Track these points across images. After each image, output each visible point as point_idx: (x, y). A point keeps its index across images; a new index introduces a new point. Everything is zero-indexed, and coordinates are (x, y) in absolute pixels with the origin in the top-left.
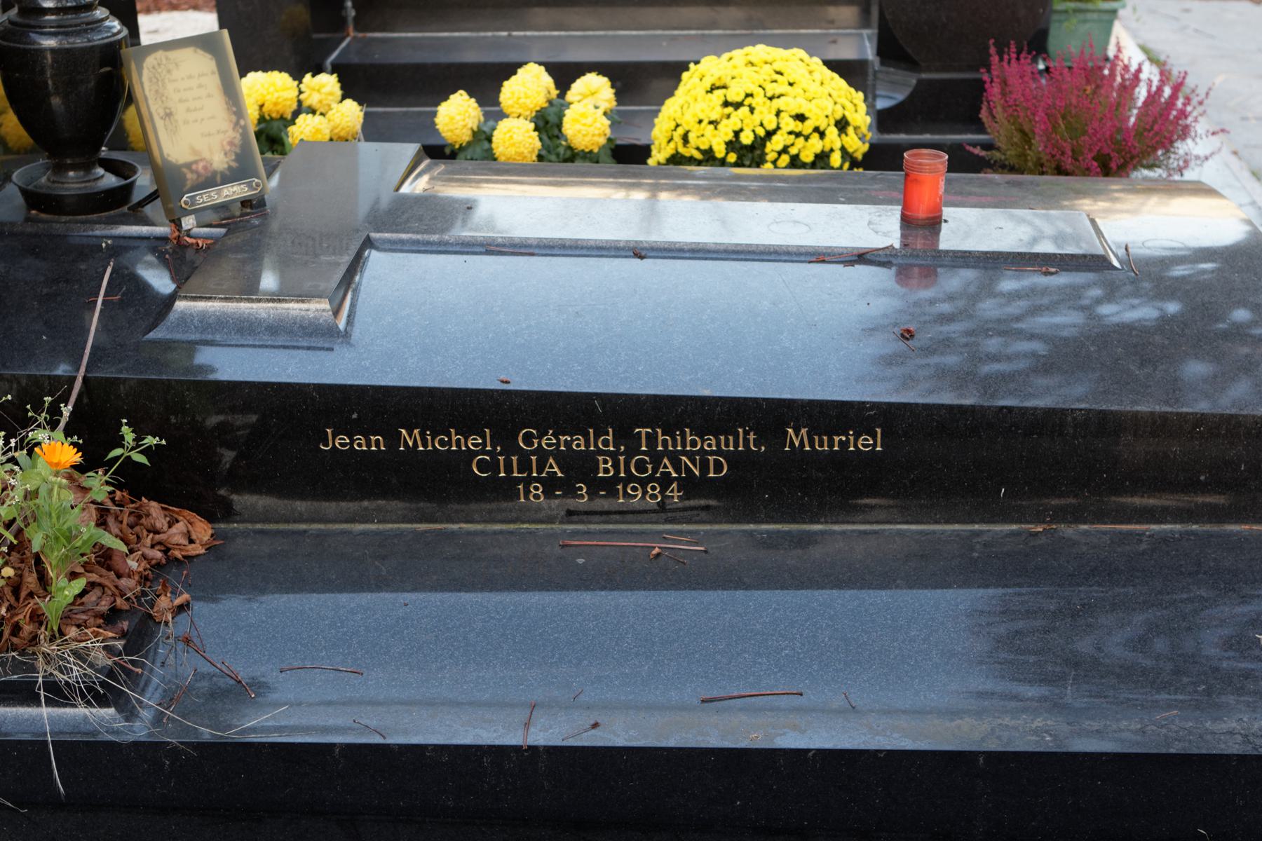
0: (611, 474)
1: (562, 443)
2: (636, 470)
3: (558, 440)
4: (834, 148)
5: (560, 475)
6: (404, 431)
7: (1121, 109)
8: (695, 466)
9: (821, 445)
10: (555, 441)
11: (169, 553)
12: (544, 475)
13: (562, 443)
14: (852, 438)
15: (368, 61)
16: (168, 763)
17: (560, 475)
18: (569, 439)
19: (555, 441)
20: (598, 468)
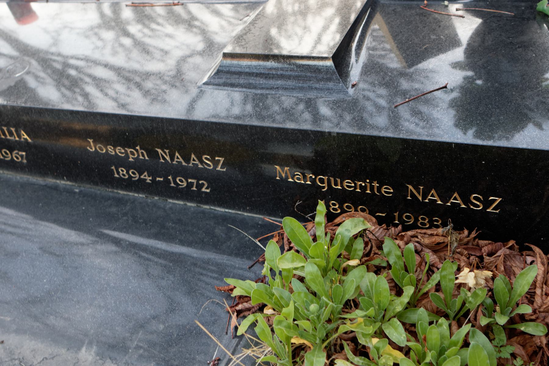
0: (211, 168)
1: (358, 187)
2: (321, 183)
3: (355, 184)
4: (501, 353)
5: (439, 202)
6: (410, 187)
7: (208, 45)
8: (419, 193)
9: (336, 184)
10: (353, 185)
11: (66, 69)
12: (427, 201)
13: (358, 187)
14: (368, 185)
15: (191, 118)
16: (286, 168)
17: (439, 202)
18: (363, 185)
19: (353, 185)
20: (427, 197)
